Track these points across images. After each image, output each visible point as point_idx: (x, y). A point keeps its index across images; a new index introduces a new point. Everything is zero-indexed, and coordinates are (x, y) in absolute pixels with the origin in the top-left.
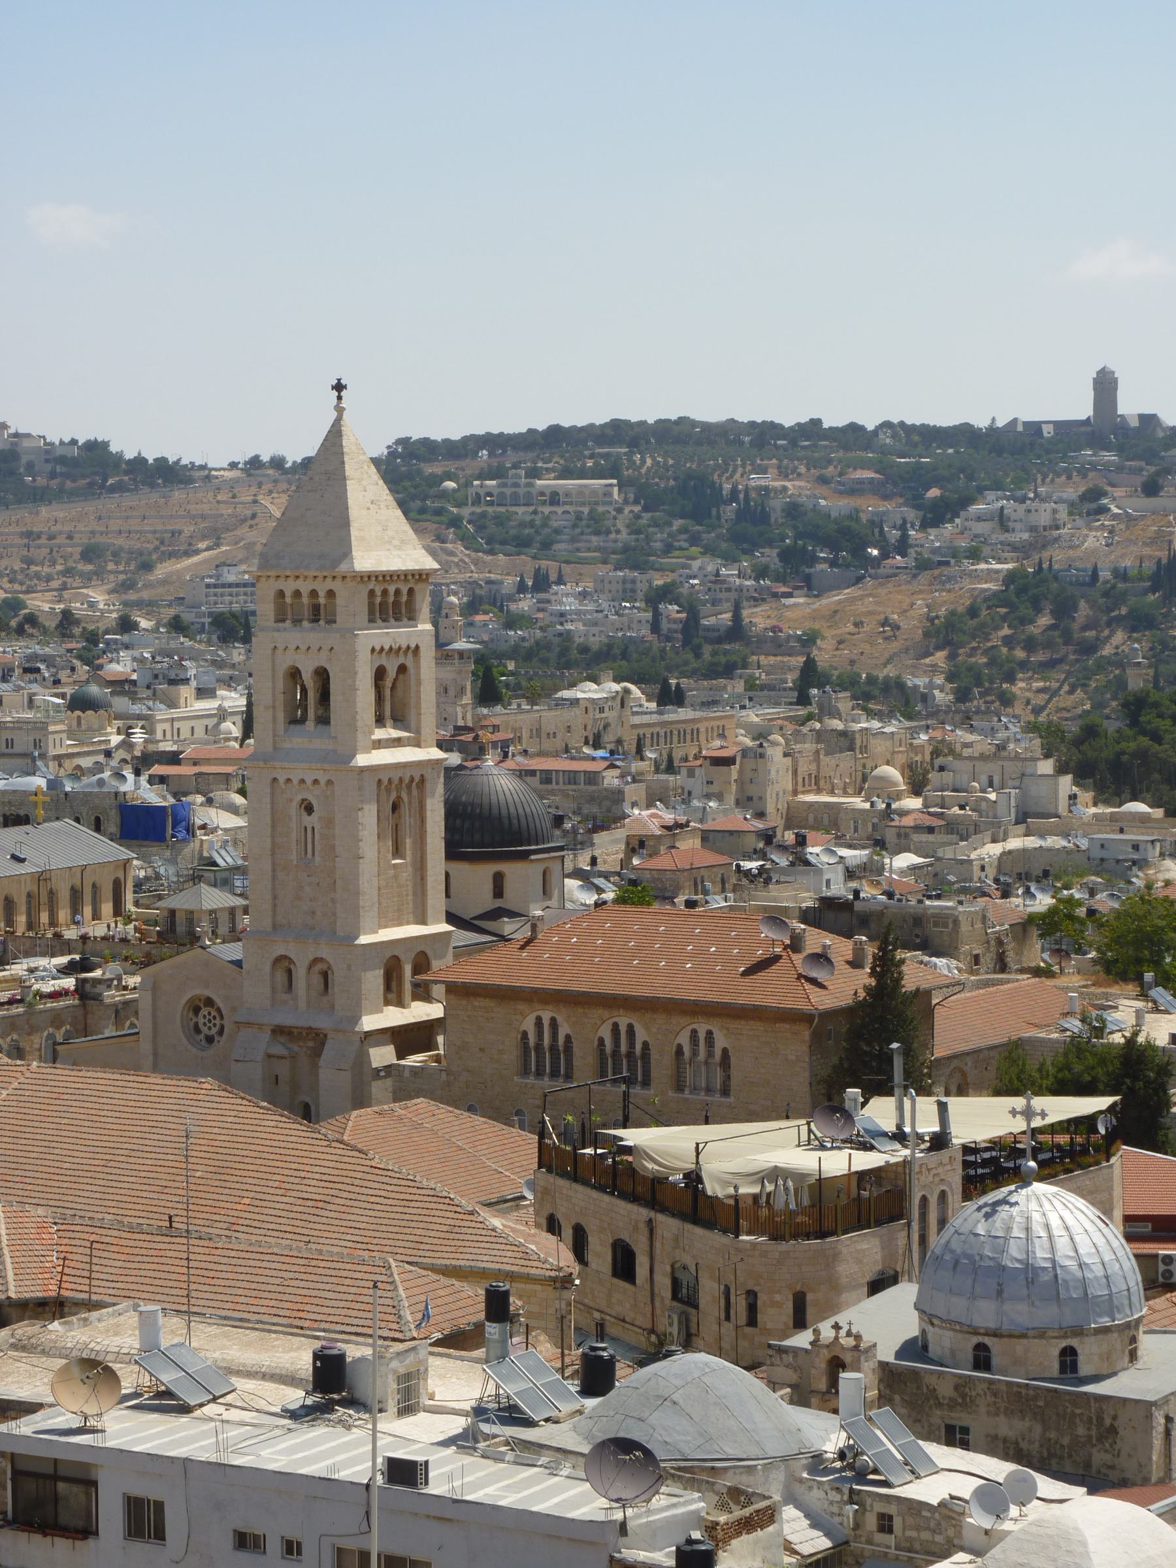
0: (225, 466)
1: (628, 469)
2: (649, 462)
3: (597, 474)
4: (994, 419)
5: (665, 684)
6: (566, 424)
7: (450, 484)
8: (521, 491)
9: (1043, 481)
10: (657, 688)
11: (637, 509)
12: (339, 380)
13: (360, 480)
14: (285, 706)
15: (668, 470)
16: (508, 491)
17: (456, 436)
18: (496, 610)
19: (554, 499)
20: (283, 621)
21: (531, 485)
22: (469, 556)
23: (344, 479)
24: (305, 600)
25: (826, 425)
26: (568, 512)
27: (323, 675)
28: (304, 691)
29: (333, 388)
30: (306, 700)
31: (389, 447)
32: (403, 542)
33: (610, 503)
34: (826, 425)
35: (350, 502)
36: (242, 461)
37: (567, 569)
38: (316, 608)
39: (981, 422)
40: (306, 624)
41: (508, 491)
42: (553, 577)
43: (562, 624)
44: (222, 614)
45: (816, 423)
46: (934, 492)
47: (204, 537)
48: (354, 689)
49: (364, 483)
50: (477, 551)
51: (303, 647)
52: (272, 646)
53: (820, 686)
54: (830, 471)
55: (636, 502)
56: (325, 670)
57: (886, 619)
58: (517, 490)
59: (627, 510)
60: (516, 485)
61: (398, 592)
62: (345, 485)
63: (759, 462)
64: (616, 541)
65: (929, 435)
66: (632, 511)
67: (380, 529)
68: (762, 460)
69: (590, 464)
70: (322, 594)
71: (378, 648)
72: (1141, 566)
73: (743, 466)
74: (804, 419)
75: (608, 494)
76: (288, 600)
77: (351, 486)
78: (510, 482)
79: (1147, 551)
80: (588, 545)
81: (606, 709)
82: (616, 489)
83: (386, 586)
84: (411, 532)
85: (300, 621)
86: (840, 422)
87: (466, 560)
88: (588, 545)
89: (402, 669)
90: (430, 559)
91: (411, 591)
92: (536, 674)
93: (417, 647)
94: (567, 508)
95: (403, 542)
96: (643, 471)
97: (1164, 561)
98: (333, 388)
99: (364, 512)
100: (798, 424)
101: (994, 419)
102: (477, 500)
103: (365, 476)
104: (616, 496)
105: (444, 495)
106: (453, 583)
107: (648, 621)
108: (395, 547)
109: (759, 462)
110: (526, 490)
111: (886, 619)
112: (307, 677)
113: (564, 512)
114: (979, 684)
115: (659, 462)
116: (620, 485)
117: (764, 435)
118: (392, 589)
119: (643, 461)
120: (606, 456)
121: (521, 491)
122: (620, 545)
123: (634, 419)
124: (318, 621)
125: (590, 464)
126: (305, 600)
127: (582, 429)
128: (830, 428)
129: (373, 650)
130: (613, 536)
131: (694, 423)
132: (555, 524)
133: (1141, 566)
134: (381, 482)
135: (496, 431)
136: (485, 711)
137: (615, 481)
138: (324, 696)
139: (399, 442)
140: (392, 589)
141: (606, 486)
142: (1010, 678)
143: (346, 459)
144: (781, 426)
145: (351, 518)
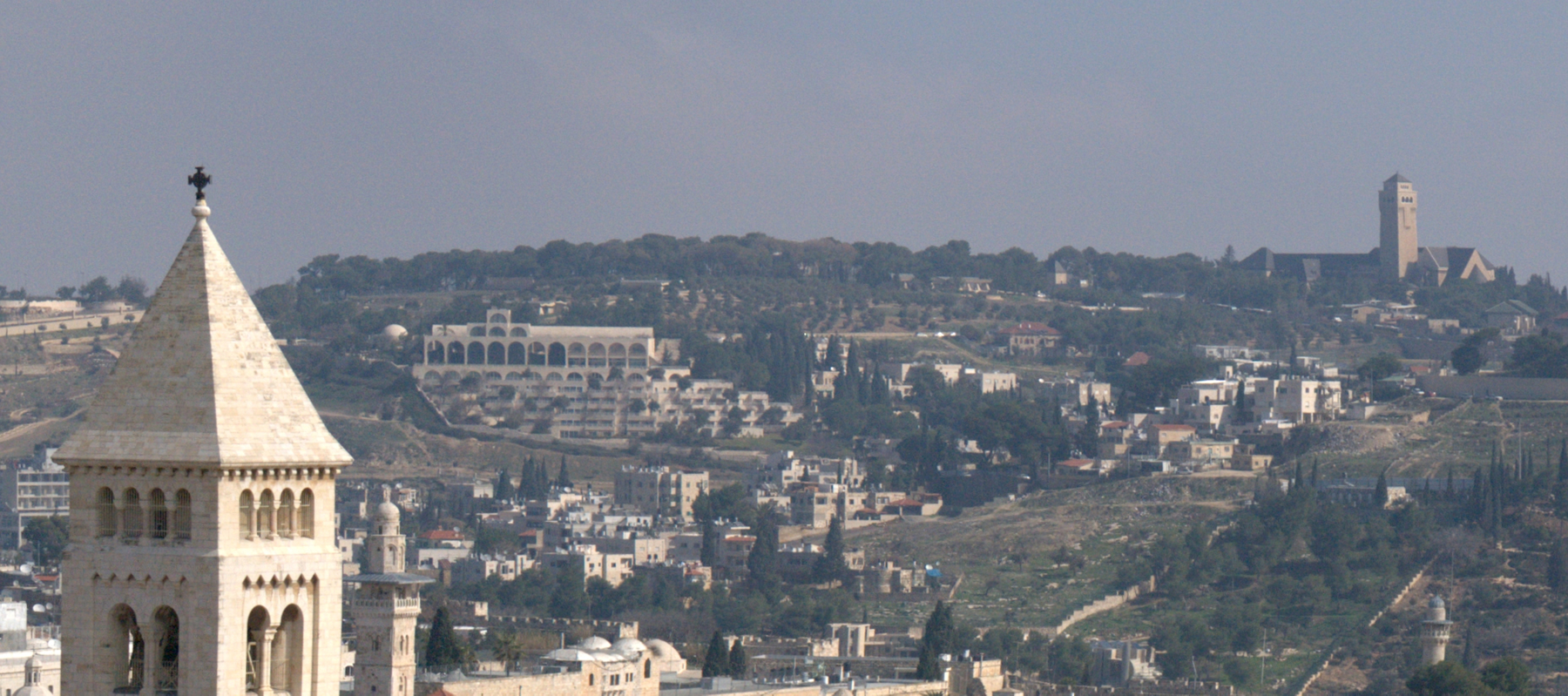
0: (53, 294)
1: (669, 311)
2: (702, 299)
3: (620, 318)
4: (1230, 250)
5: (717, 644)
6: (575, 239)
7: (398, 330)
8: (506, 341)
9: (1305, 343)
10: (700, 647)
11: (684, 372)
12: (199, 169)
13: (231, 322)
14: (987, 506)
15: (730, 314)
16: (486, 341)
17: (406, 255)
18: (462, 523)
19: (557, 353)
20: (110, 535)
21: (520, 332)
22: (424, 439)
23: (206, 319)
24: (145, 504)
25: (974, 251)
26: (578, 376)
27: (169, 619)
28: (139, 643)
29: (191, 181)
30: (142, 657)
31: (302, 270)
32: (295, 418)
33: (643, 363)
34: (974, 251)
35: (215, 356)
36: (78, 287)
37: (573, 461)
38: (160, 519)
39: (1210, 252)
40: (144, 541)
41: (486, 341)
42: (552, 476)
43: (565, 546)
44: (40, 521)
45: (958, 247)
46: (1138, 359)
47: (19, 403)
48: (213, 642)
49: (238, 327)
50: (433, 431)
51: (140, 577)
52: (93, 573)
53: (957, 651)
54: (980, 322)
55: (682, 363)
56: (173, 614)
57: (1063, 550)
58: (500, 339)
59: (668, 373)
60: (498, 331)
61: (287, 494)
62: (208, 330)
63: (871, 305)
64: (650, 422)
65: (1135, 273)
66: (674, 377)
67: (260, 397)
68: (876, 302)
69: (611, 301)
70: (169, 496)
71: (254, 580)
72: (1450, 480)
73: (847, 310)
74: (940, 241)
75: (639, 349)
76: (119, 503)
77: (217, 332)
78: (489, 326)
79: (1459, 457)
80: (607, 428)
81: (622, 679)
82: (651, 343)
83: (269, 484)
84: (307, 403)
85: (138, 535)
86: (997, 249)
87: (421, 445)
88: (607, 428)
89: (292, 613)
90: (336, 445)
91: (307, 494)
92: (521, 622)
93: (315, 580)
94: (577, 369)
95: (295, 418)
96: (694, 314)
97: (1486, 473)
98: (191, 181)
99: (237, 371)
100: (931, 249)
101: (1230, 250)
102: (437, 356)
103: (239, 316)
104: (651, 352)
105: (389, 348)
106: (399, 480)
107: (697, 545)
108: (284, 425)
109: (871, 305)
110: (515, 339)
111: (1063, 550)
112: (145, 618)
113: (571, 376)
114: (1200, 652)
115: (717, 302)
116: (657, 336)
117: (873, 267)
118: (277, 489)
119: (693, 299)
120: (634, 291)
121: (506, 341)
122: (657, 429)
123: (680, 234)
124: (162, 536)
125: (611, 301)
126: (145, 504)
127: (599, 250)
128: (981, 257)
129: (247, 583)
130: (647, 413)
131: (771, 244)
132: (555, 392)
133: (1450, 480)
134: (263, 326)
135: (467, 248)
136: (435, 678)
137: (649, 331)
138: (170, 653)
139: (319, 262)
140: (277, 489)
141: (639, 337)
142: (1245, 641)
143: (210, 289)
144: (905, 252)
145: (216, 381)
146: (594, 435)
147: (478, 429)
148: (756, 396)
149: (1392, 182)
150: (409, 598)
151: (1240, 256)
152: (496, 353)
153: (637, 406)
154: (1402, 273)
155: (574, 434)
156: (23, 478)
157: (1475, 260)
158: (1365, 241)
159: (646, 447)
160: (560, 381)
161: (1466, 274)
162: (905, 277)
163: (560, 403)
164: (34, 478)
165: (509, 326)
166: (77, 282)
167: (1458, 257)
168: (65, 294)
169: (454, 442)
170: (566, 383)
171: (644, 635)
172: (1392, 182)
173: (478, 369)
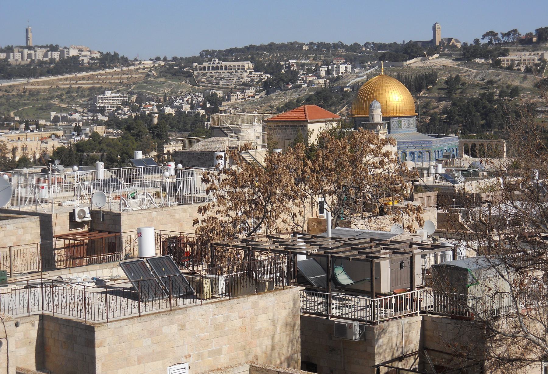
41: (211, 66)
60: (214, 63)
78: (212, 62)
146: (228, 85)
147: (203, 84)
148: (267, 75)
149: (435, 25)
150: (267, 141)
151: (406, 42)
152: (213, 68)
153: (239, 78)
154: (438, 44)
155: (225, 85)
156: (99, 98)
157: (453, 41)
158: (430, 38)
159: (238, 87)
160: (224, 74)
161: (451, 44)
162: (324, 50)
163: (223, 78)
164: (102, 98)
165: (216, 62)
166: (153, 57)
167: (450, 40)
168: (151, 60)
169: (197, 87)
170: (226, 74)
171: (171, 114)
172: (435, 25)
173: (205, 72)
